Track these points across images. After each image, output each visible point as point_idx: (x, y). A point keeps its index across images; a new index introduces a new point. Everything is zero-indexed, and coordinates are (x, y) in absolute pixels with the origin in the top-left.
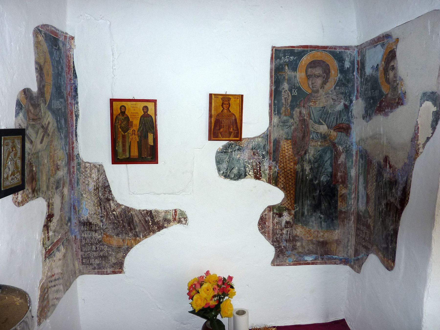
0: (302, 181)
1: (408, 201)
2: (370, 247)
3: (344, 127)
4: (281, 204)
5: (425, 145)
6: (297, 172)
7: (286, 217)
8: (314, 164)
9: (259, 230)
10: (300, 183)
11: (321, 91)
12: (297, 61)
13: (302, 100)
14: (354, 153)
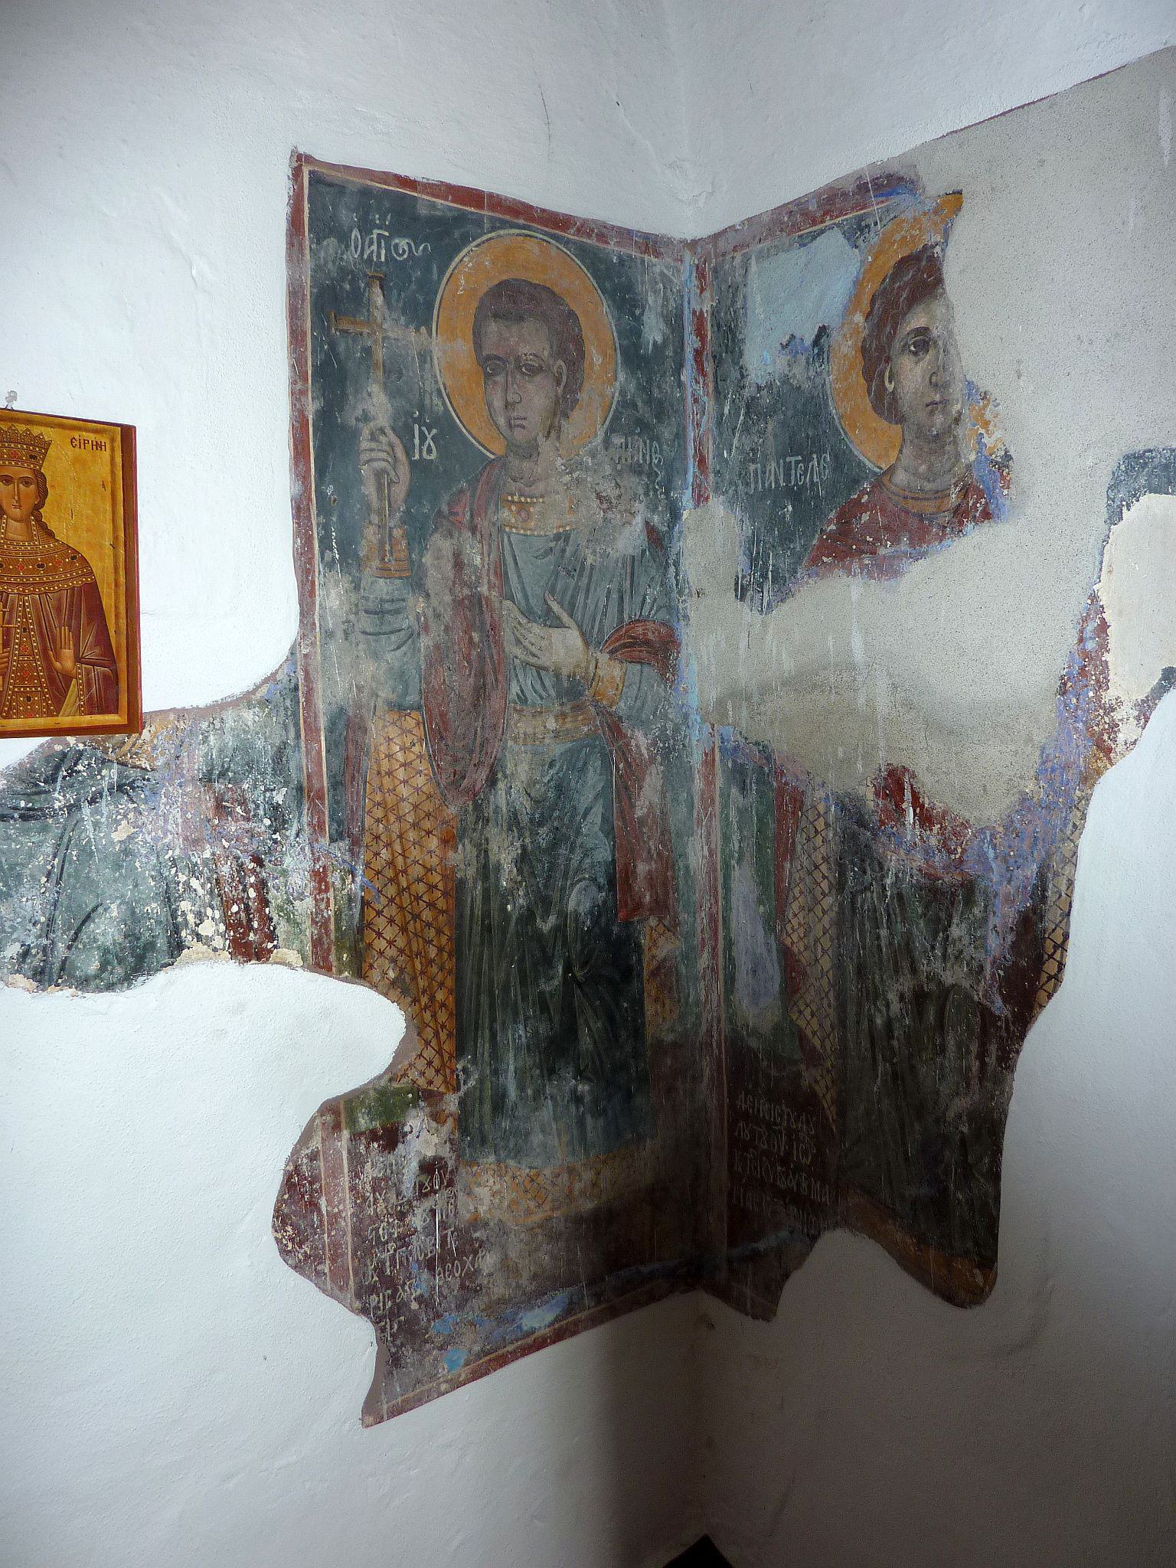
0: (487, 929)
1: (1057, 978)
2: (826, 1199)
3: (650, 636)
4: (393, 1073)
5: (1151, 709)
6: (462, 883)
7: (423, 1138)
8: (534, 834)
9: (284, 1252)
10: (476, 939)
11: (546, 446)
12: (427, 270)
13: (461, 491)
14: (696, 759)
